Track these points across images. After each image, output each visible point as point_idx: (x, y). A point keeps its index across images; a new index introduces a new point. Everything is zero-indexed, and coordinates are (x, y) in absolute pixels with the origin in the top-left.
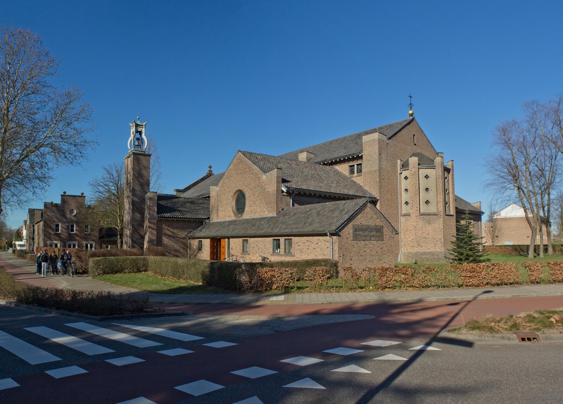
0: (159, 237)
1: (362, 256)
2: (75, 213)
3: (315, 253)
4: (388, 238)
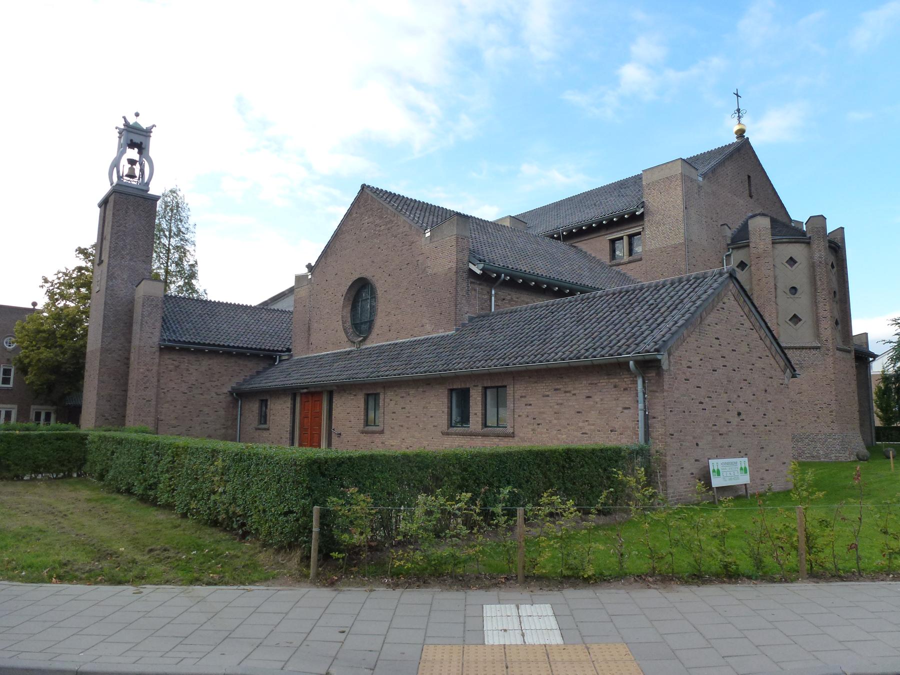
0: (165, 391)
1: (723, 436)
2: (7, 347)
3: (581, 424)
4: (776, 386)
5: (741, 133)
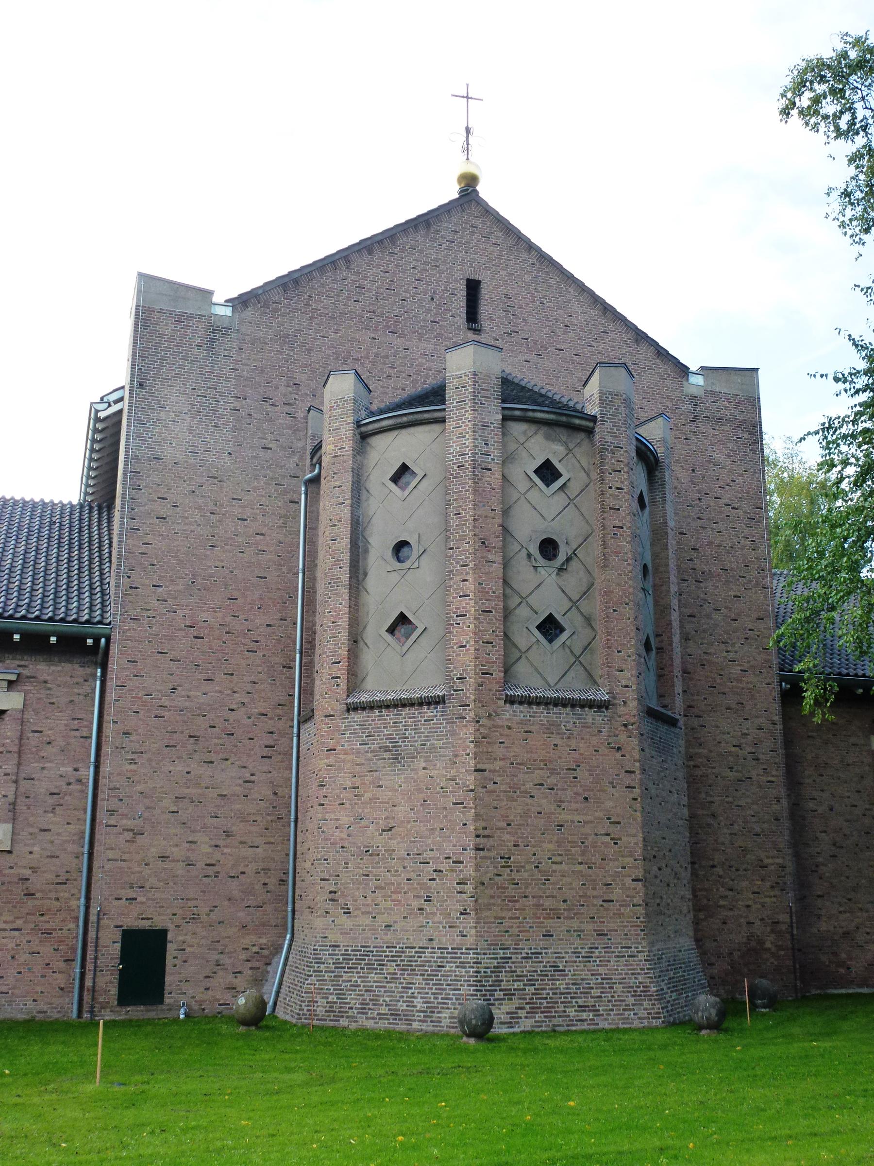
5: (469, 183)
